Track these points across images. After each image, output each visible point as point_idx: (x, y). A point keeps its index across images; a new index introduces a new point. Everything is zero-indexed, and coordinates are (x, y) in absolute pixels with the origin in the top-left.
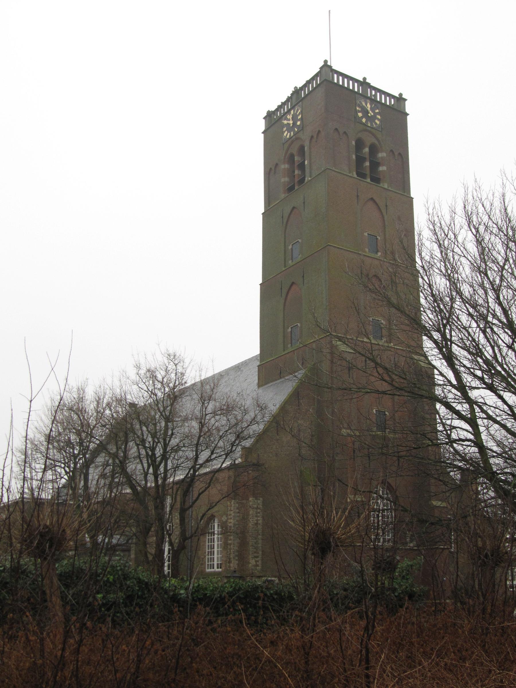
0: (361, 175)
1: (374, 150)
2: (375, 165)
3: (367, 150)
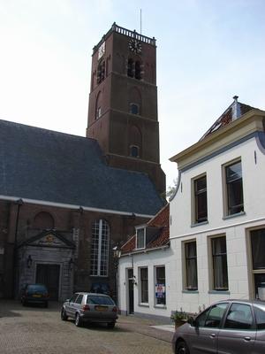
0: (130, 74)
1: (138, 64)
2: (138, 70)
3: (134, 64)
